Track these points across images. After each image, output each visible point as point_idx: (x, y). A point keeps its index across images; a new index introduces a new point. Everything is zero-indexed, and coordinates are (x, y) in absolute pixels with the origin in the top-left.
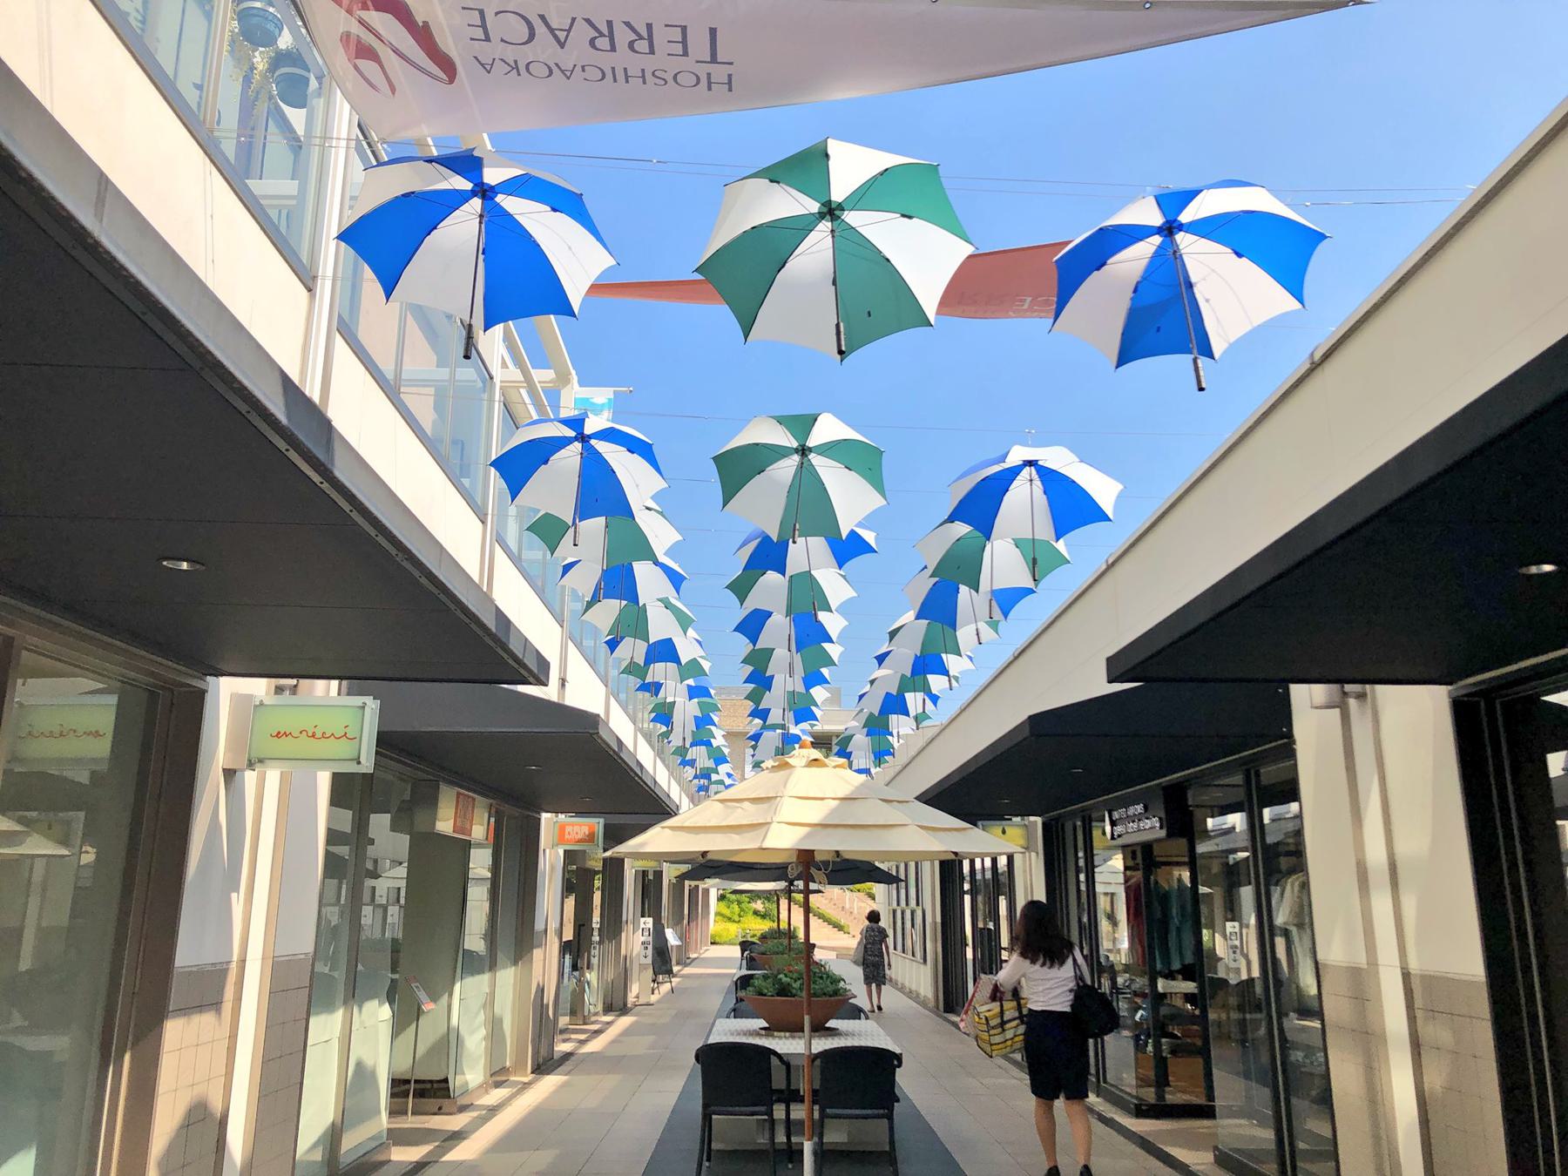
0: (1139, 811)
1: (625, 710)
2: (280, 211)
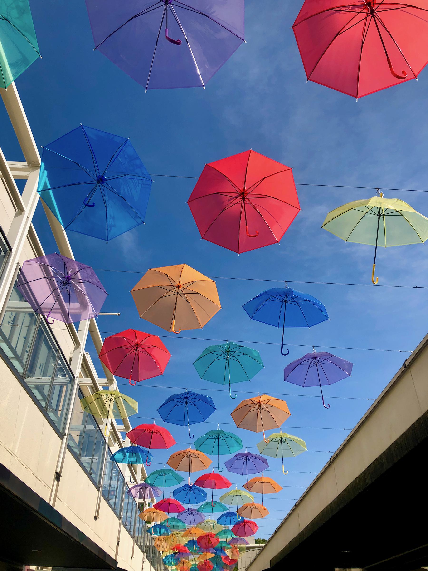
1: (129, 532)
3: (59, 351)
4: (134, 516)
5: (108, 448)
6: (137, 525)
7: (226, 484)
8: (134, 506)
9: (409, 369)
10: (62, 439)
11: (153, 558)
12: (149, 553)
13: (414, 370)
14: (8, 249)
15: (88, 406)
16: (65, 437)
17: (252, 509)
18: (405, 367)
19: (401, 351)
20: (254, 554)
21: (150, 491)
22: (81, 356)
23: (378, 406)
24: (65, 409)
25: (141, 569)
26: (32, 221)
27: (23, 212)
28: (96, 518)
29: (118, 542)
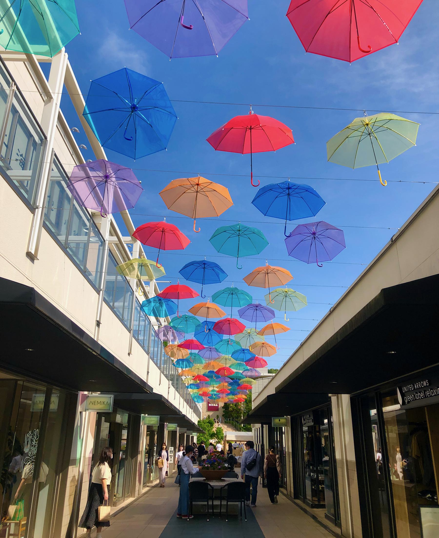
0: (425, 384)
1: (156, 364)
2: (28, 181)
3: (91, 220)
4: (159, 352)
5: (109, 250)
6: (163, 358)
7: (240, 328)
8: (159, 343)
9: (395, 243)
10: (99, 294)
11: (177, 384)
12: (174, 381)
13: (399, 244)
14: (43, 138)
15: (83, 204)
16: (101, 292)
17: (262, 348)
18: (392, 241)
19: (389, 229)
20: (266, 381)
21: (186, 364)
22: (109, 221)
23: (375, 265)
24: (99, 270)
25: (168, 393)
26: (60, 107)
27: (51, 100)
28: (129, 354)
29: (148, 372)
